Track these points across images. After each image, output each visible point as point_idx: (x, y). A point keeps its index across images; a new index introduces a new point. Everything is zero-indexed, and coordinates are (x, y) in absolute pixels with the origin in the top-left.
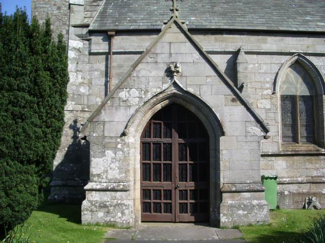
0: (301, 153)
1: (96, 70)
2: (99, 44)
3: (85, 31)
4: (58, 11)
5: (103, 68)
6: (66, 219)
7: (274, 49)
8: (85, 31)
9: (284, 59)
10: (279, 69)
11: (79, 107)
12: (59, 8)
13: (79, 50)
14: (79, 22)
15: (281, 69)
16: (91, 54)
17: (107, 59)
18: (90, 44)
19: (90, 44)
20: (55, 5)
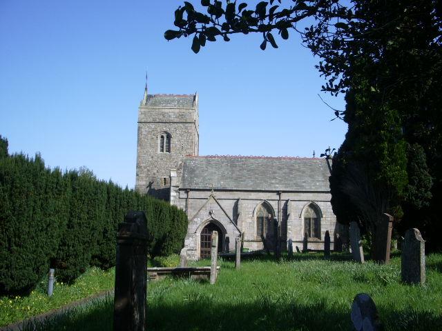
2: (183, 195)
7: (254, 198)
12: (152, 157)
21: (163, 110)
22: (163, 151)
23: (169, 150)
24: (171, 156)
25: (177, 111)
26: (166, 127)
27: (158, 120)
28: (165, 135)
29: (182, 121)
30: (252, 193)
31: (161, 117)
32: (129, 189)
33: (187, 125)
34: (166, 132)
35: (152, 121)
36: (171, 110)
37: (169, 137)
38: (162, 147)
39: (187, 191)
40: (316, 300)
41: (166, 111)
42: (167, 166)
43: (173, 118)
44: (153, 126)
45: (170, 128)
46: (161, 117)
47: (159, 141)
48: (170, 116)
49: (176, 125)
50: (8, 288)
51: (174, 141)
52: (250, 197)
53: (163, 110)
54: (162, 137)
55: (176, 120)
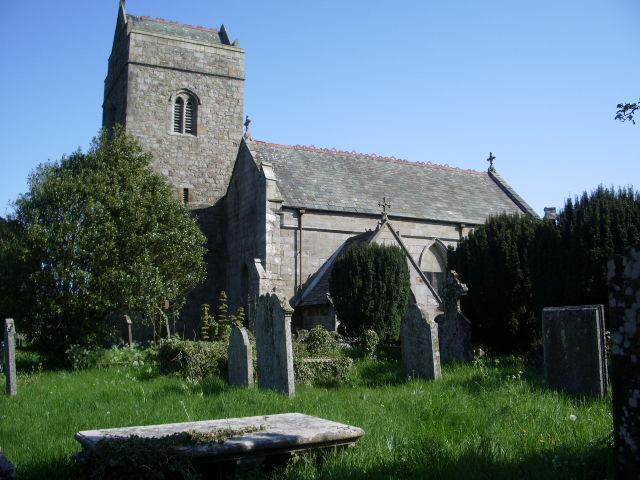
0: (510, 201)
1: (287, 243)
2: (290, 220)
3: (279, 206)
4: (158, 145)
5: (293, 242)
6: (589, 195)
7: (421, 234)
8: (279, 206)
9: (426, 242)
10: (202, 73)
11: (275, 276)
12: (159, 142)
13: (273, 223)
14: (273, 198)
15: (201, 71)
16: (282, 227)
17: (296, 234)
18: (282, 218)
19: (282, 218)
20: (154, 136)
21: (183, 46)
22: (180, 131)
23: (193, 130)
24: (197, 143)
25: (212, 51)
26: (187, 80)
27: (171, 65)
28: (185, 98)
29: (220, 72)
30: (418, 225)
31: (179, 58)
32: (589, 195)
33: (230, 82)
34: (187, 91)
35: (158, 64)
36: (198, 48)
37: (194, 102)
38: (179, 122)
39: (298, 212)
40: (433, 460)
41: (189, 47)
42: (191, 163)
43: (200, 65)
44: (161, 74)
45: (199, 85)
46: (179, 58)
47: (172, 108)
48: (196, 60)
49: (209, 80)
50: (373, 229)
51: (205, 111)
52: (414, 232)
53: (183, 46)
54: (179, 101)
55: (208, 69)
